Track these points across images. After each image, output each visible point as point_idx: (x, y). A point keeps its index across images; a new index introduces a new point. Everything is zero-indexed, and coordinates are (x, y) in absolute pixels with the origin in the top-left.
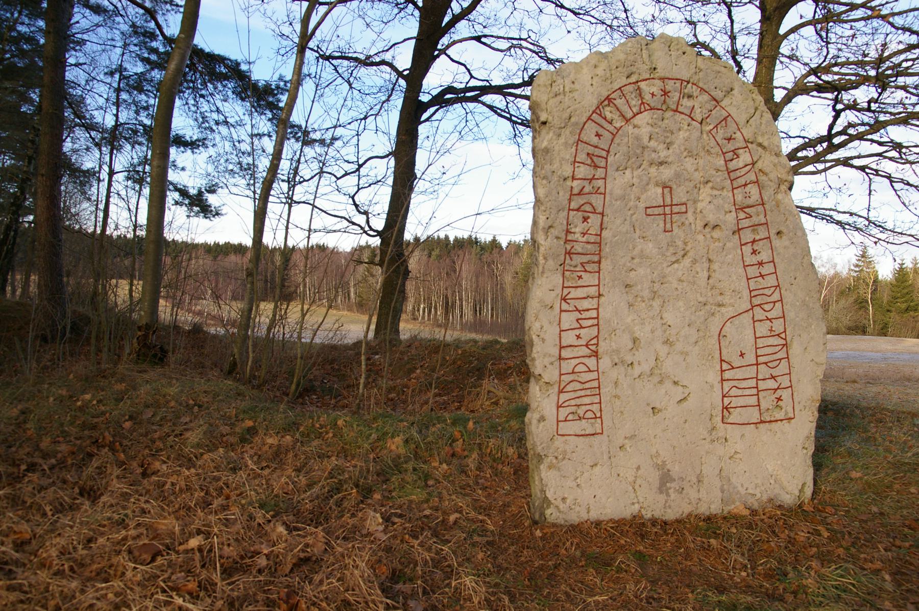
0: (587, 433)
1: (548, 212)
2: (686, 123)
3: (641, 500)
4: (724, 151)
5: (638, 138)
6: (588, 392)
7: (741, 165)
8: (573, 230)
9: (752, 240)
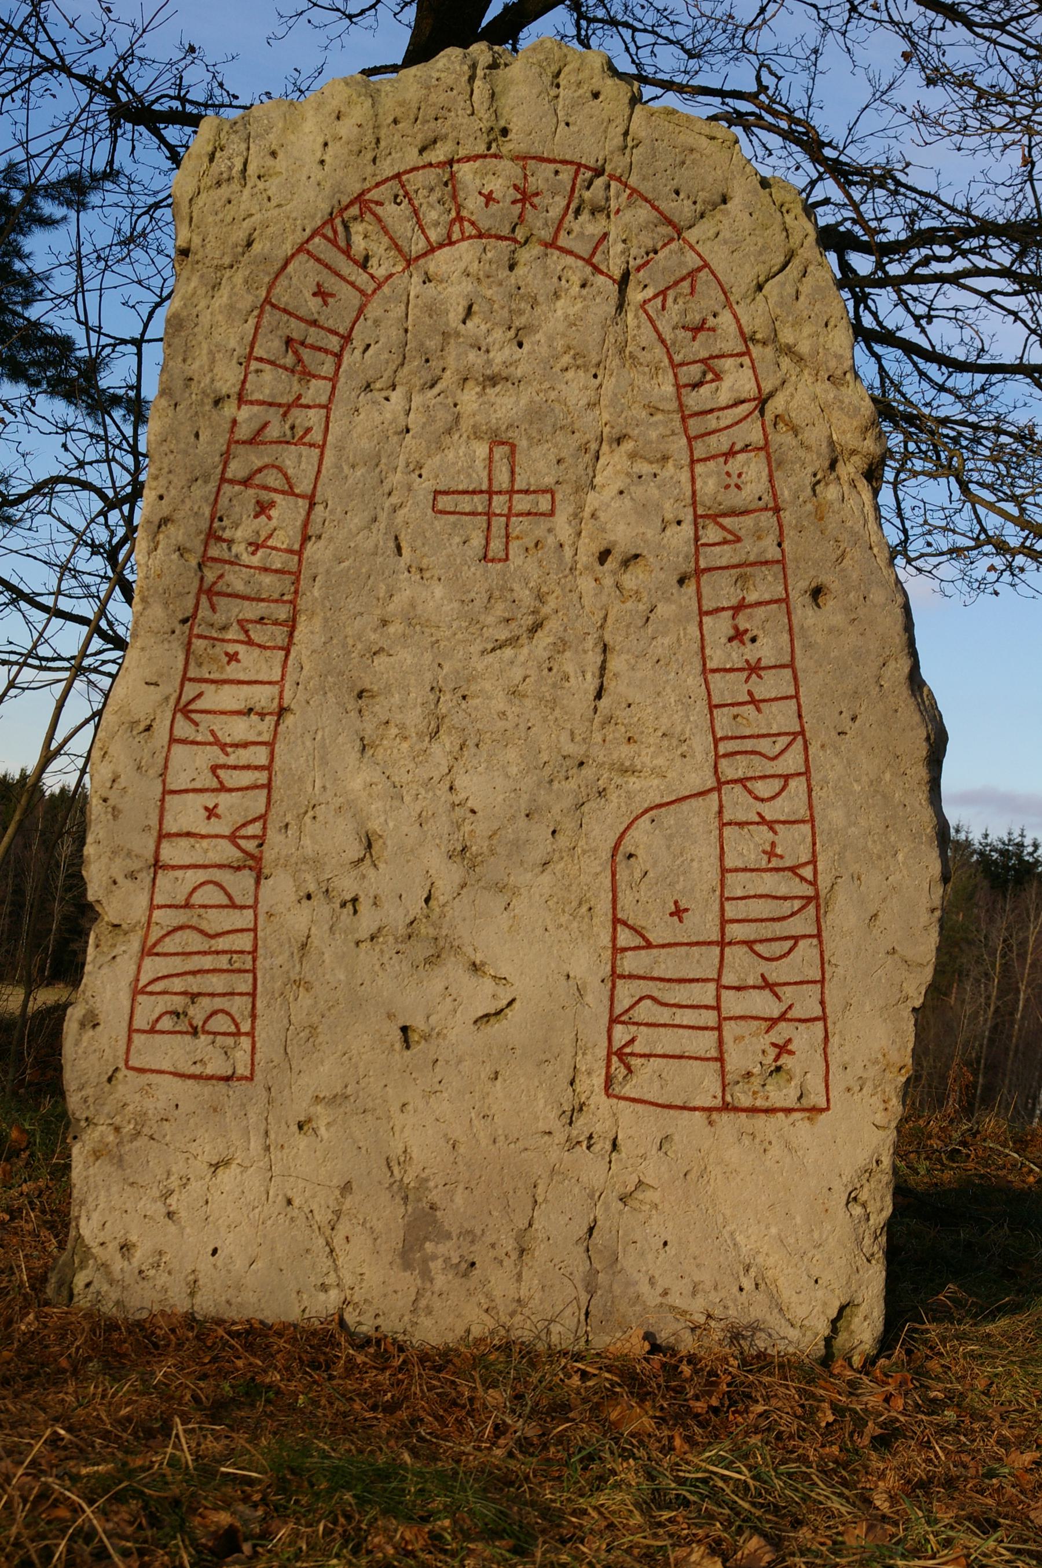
0: (209, 1071)
1: (163, 481)
2: (576, 280)
3: (348, 1280)
4: (678, 358)
5: (432, 310)
6: (223, 962)
7: (724, 397)
8: (227, 534)
9: (734, 602)
